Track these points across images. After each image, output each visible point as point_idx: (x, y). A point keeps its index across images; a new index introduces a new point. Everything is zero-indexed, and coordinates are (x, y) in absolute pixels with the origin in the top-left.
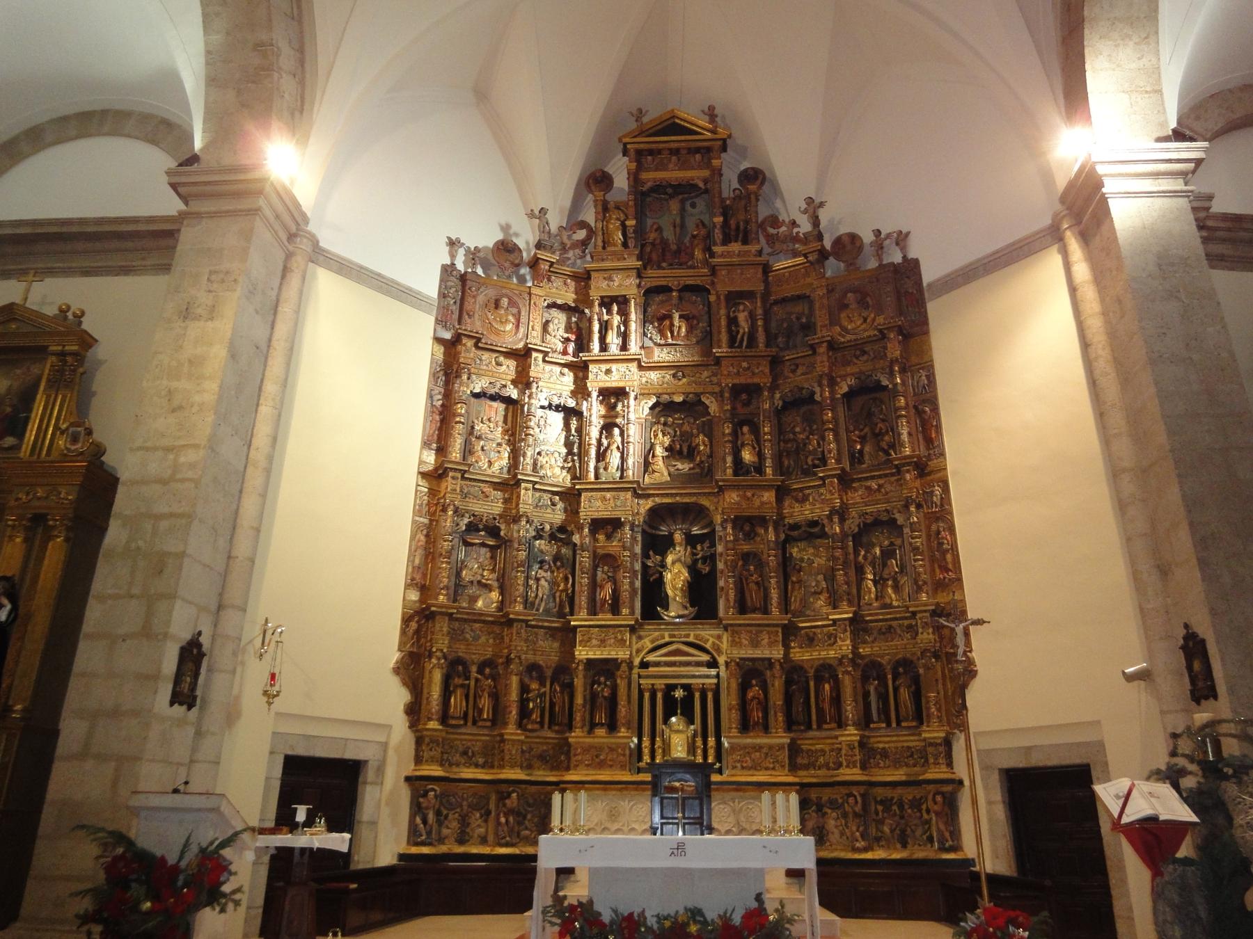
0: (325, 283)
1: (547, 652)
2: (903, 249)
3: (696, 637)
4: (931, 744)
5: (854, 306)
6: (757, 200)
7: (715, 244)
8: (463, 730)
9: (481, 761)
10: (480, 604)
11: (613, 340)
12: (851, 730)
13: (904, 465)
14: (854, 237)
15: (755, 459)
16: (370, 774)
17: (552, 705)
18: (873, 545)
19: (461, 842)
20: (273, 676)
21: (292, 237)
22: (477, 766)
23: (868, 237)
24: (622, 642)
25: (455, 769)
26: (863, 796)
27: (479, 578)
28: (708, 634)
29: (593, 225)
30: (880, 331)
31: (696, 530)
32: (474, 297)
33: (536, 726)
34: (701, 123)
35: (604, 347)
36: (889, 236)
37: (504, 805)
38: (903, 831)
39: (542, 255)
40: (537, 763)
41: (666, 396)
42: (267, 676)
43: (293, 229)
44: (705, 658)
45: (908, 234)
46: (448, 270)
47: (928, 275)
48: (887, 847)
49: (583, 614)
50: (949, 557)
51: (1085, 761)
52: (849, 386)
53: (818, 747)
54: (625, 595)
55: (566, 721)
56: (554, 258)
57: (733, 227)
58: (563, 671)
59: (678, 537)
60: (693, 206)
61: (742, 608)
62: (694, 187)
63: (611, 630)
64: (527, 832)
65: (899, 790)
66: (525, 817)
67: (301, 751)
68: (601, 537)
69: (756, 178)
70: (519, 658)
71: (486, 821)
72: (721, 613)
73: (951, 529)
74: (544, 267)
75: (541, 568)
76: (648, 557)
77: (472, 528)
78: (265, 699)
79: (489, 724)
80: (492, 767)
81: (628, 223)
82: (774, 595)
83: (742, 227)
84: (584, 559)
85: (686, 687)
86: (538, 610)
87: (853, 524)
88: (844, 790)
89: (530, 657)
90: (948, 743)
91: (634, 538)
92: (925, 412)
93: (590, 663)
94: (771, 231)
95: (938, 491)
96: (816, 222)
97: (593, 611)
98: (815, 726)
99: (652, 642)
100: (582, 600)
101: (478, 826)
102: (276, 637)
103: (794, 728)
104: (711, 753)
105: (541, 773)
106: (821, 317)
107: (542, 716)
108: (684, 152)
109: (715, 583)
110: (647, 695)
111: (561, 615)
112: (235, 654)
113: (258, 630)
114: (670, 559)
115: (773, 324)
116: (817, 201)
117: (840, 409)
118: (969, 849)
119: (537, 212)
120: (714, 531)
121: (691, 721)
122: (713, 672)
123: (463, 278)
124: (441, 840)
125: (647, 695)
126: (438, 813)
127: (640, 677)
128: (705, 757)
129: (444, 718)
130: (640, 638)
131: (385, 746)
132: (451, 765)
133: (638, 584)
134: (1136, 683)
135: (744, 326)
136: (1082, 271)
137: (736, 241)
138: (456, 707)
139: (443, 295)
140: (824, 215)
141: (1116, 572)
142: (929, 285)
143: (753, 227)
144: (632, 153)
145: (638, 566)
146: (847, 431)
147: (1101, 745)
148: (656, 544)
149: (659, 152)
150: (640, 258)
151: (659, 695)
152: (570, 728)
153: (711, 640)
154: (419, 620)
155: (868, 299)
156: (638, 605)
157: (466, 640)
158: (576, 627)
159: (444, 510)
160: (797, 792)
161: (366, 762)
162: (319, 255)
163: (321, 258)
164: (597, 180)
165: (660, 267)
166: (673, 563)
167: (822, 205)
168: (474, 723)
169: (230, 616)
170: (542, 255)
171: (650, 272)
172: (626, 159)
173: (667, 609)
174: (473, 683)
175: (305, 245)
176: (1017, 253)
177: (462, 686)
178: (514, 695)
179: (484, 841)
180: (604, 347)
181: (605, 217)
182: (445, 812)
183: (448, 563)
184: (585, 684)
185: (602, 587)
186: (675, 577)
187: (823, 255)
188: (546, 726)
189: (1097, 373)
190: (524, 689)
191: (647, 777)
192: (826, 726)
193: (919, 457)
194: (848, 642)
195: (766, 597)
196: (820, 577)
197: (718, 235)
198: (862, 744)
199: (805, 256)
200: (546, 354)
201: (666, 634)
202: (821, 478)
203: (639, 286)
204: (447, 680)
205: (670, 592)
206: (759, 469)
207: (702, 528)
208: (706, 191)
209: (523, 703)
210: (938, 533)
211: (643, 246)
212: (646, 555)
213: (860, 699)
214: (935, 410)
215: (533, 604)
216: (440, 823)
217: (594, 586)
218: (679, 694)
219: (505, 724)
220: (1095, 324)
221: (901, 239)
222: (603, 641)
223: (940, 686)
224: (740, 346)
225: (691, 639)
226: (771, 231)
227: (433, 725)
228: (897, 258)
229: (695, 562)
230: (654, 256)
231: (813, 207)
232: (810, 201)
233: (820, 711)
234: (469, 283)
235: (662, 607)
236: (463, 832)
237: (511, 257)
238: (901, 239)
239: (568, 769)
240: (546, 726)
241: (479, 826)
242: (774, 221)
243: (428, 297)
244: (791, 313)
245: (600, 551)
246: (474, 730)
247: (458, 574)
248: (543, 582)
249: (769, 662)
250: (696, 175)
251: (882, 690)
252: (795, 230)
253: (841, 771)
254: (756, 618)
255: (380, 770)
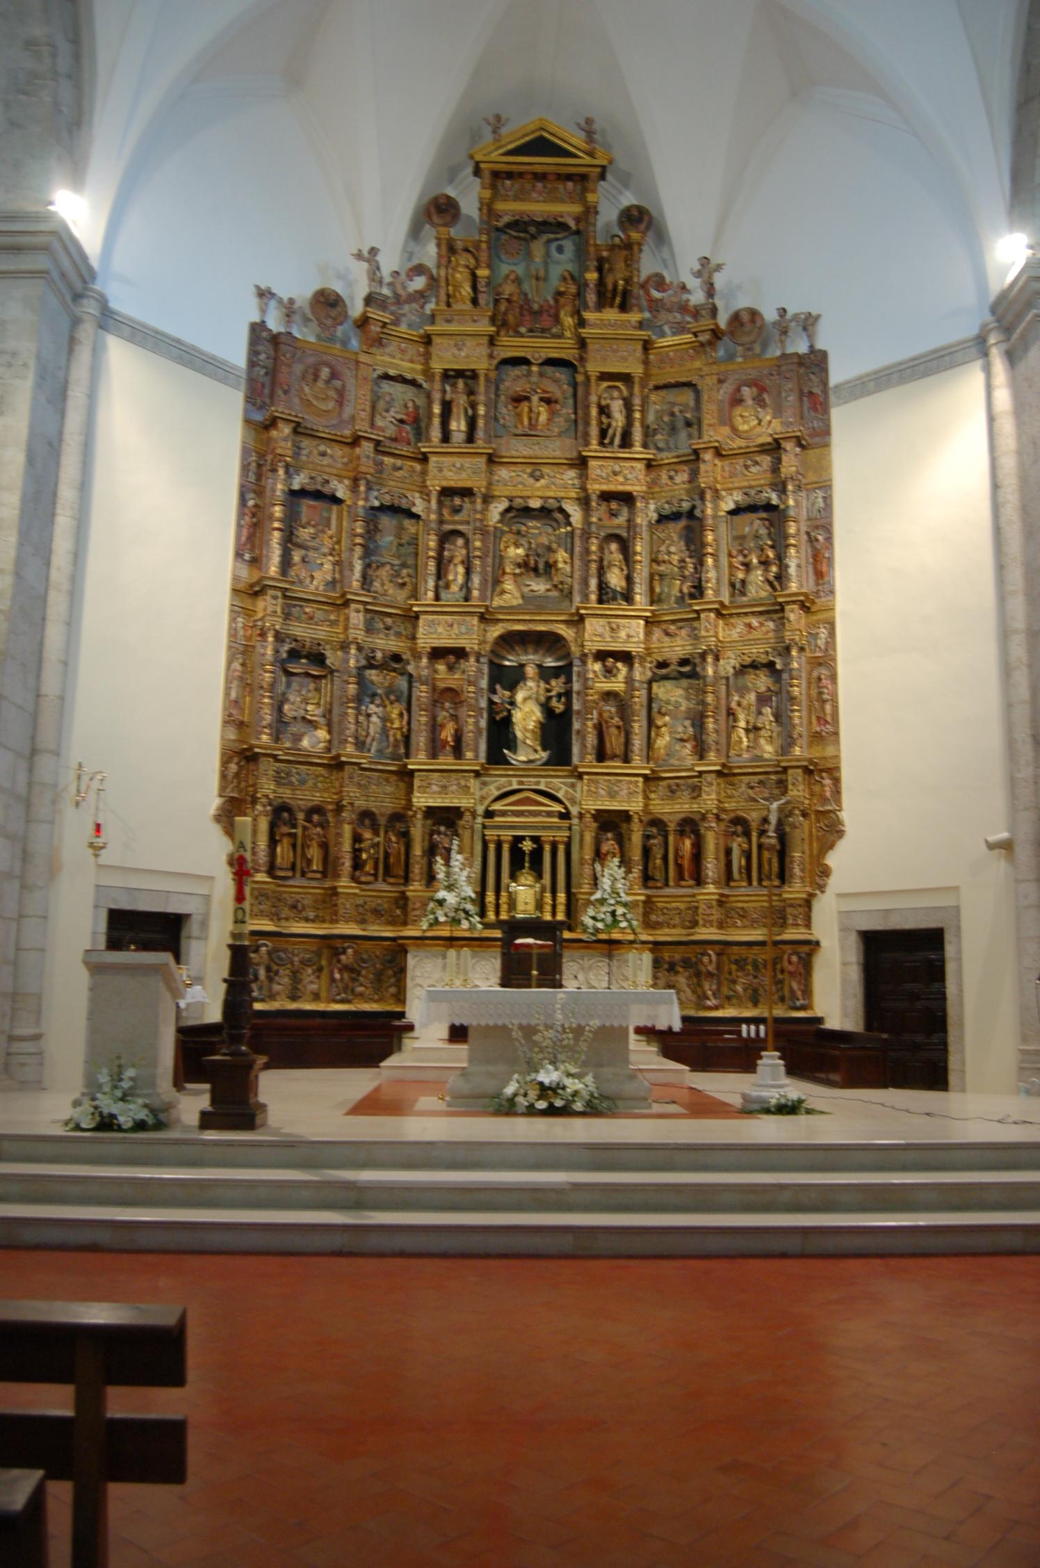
0: (122, 363)
1: (383, 799)
2: (811, 337)
3: (547, 784)
4: (792, 906)
5: (750, 402)
6: (641, 250)
7: (586, 307)
8: (291, 882)
9: (311, 915)
10: (305, 743)
11: (458, 425)
12: (711, 888)
13: (788, 603)
14: (754, 314)
15: (624, 584)
16: (193, 928)
17: (387, 855)
18: (748, 690)
19: (294, 998)
20: (98, 828)
21: (77, 297)
22: (307, 920)
23: (770, 315)
24: (466, 789)
25: (284, 923)
26: (718, 955)
27: (302, 713)
28: (559, 784)
29: (434, 272)
30: (776, 440)
31: (550, 662)
32: (289, 366)
33: (371, 878)
34: (574, 141)
35: (446, 438)
36: (796, 317)
37: (339, 961)
38: (755, 991)
39: (374, 313)
40: (369, 917)
41: (520, 500)
42: (91, 829)
43: (78, 286)
44: (558, 808)
45: (818, 317)
46: (257, 329)
47: (838, 374)
48: (740, 1005)
49: (422, 756)
50: (828, 707)
51: (940, 925)
52: (736, 502)
53: (674, 905)
54: (468, 736)
55: (402, 873)
56: (386, 317)
57: (610, 287)
58: (399, 819)
59: (530, 671)
60: (560, 250)
61: (601, 756)
62: (562, 226)
63: (453, 775)
64: (362, 989)
65: (756, 949)
66: (359, 974)
67: (125, 904)
68: (441, 667)
69: (640, 220)
70: (352, 804)
71: (318, 977)
72: (575, 760)
73: (833, 677)
74: (375, 329)
75: (372, 703)
76: (494, 691)
77: (294, 655)
78: (91, 851)
79: (319, 876)
80: (324, 921)
81: (480, 273)
82: (638, 742)
83: (620, 288)
84: (422, 693)
85: (535, 839)
86: (369, 751)
87: (728, 665)
88: (698, 949)
89: (361, 804)
90: (808, 903)
91: (480, 670)
92: (817, 540)
93: (430, 812)
94: (656, 294)
95: (823, 633)
96: (710, 291)
97: (433, 755)
98: (671, 883)
99: (498, 789)
100: (421, 740)
101: (310, 983)
102: (95, 785)
103: (651, 883)
104: (561, 909)
105: (376, 928)
106: (710, 415)
107: (376, 867)
108: (551, 177)
109: (570, 724)
110: (492, 847)
111: (395, 757)
112: (54, 802)
113: (72, 775)
114: (520, 696)
115: (651, 418)
116: (714, 262)
117: (723, 528)
118: (818, 1012)
119: (366, 254)
120: (570, 665)
121: (539, 876)
122: (565, 823)
123: (275, 339)
124: (272, 997)
125: (492, 847)
126: (268, 969)
127: (484, 827)
128: (554, 913)
129: (271, 870)
130: (484, 784)
131: (207, 898)
132: (279, 919)
133: (483, 723)
134: (997, 851)
135: (619, 419)
136: (1003, 397)
137: (612, 306)
138: (283, 858)
139: (252, 364)
140: (719, 280)
141: (993, 739)
142: (837, 387)
143: (636, 291)
144: (487, 174)
145: (483, 704)
146: (730, 555)
147: (957, 909)
148: (507, 678)
149: (521, 175)
150: (493, 320)
151: (506, 847)
152: (407, 879)
153: (564, 788)
154: (242, 758)
155: (765, 396)
156: (483, 747)
157: (291, 784)
158: (413, 771)
159: (263, 634)
160: (651, 951)
161: (188, 916)
162: (108, 319)
163: (111, 322)
164: (439, 210)
165: (518, 334)
166: (525, 699)
167: (719, 267)
168: (303, 874)
169: (45, 763)
170: (374, 313)
171: (504, 340)
172: (478, 180)
173: (515, 752)
174: (299, 831)
175: (90, 307)
176: (933, 364)
177: (290, 835)
178: (347, 846)
179: (316, 997)
180: (446, 438)
181: (449, 261)
182: (275, 968)
183: (271, 697)
184: (424, 833)
185: (442, 726)
186: (526, 716)
187: (716, 334)
188: (380, 879)
189: (1003, 520)
190: (357, 838)
191: (498, 934)
192: (683, 883)
193: (805, 595)
194: (714, 796)
195: (628, 743)
196: (687, 723)
197: (591, 298)
198: (721, 903)
199: (695, 334)
200: (378, 443)
201: (514, 780)
202: (697, 612)
203: (491, 356)
204: (273, 827)
205: (519, 734)
206: (628, 597)
207: (558, 660)
208: (580, 231)
209: (356, 853)
210: (820, 679)
211: (497, 302)
212: (493, 691)
213: (722, 856)
214: (829, 539)
215: (364, 743)
216: (270, 979)
217: (435, 727)
218: (527, 846)
219: (337, 876)
220: (1009, 463)
221: (808, 323)
222: (444, 787)
223: (806, 847)
224: (611, 443)
225: (542, 787)
226: (656, 294)
227: (261, 877)
228: (802, 347)
229: (549, 698)
230: (511, 318)
231: (707, 269)
232: (705, 261)
233: (679, 867)
234: (283, 348)
235: (509, 749)
236: (295, 989)
237: (333, 313)
238: (808, 323)
239: (405, 923)
240: (380, 879)
241: (312, 982)
242: (660, 283)
243: (234, 367)
244: (673, 404)
245: (441, 685)
246: (304, 882)
247: (280, 710)
248: (374, 719)
249: (626, 816)
250: (567, 210)
251: (745, 846)
252: (685, 296)
253: (697, 930)
254: (615, 766)
255: (204, 924)
